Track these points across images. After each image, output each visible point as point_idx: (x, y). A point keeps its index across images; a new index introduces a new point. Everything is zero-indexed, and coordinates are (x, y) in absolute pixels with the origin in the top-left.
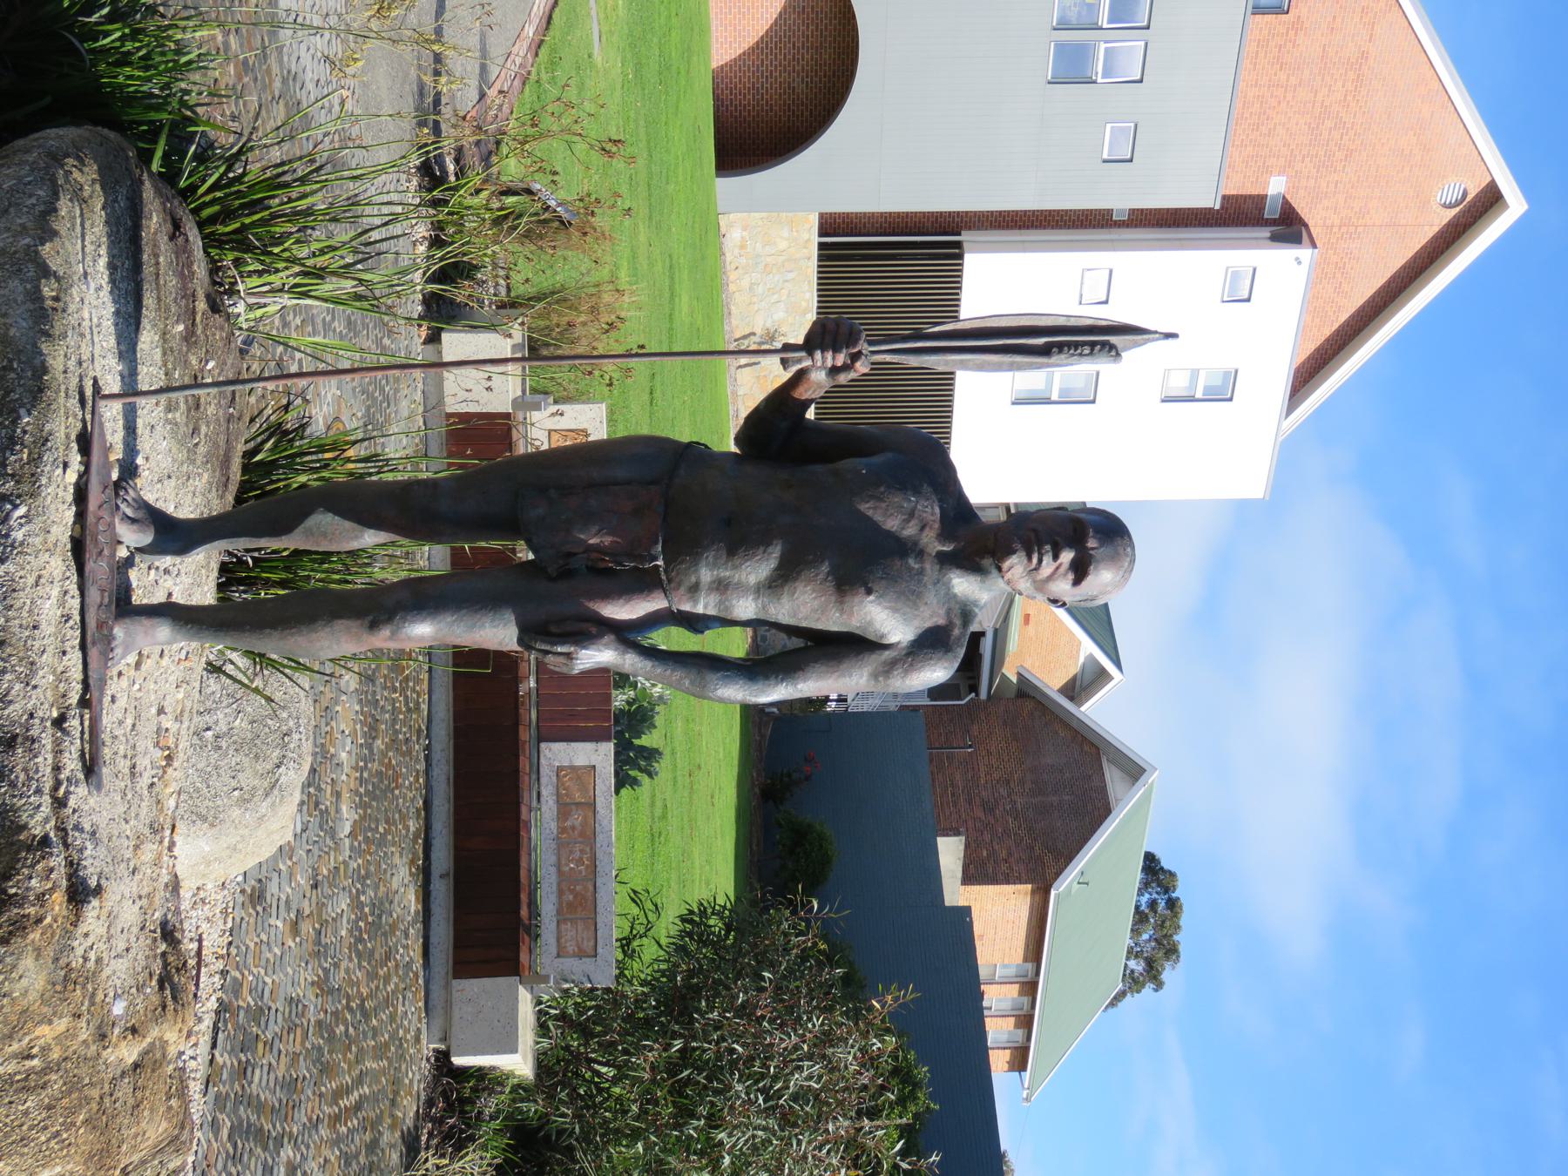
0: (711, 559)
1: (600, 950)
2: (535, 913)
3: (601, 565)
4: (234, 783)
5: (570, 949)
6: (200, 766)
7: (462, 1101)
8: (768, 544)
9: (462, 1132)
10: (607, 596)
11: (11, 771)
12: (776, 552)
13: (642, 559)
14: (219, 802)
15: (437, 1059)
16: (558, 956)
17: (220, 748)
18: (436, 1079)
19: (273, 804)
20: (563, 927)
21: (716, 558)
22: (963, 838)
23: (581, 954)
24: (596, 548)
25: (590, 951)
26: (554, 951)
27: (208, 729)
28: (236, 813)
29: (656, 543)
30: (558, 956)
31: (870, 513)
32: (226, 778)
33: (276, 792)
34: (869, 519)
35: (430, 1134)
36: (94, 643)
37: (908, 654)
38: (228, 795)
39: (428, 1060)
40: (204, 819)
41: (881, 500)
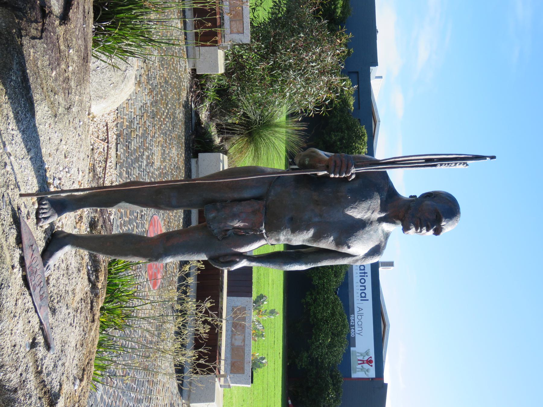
0: (284, 233)
1: (245, 31)
2: (221, 345)
3: (240, 234)
4: (110, 82)
5: (235, 31)
6: (97, 81)
7: (202, 85)
8: (308, 230)
9: (202, 94)
10: (242, 246)
11: (18, 399)
12: (311, 233)
13: (256, 231)
14: (106, 90)
15: (192, 72)
16: (231, 33)
17: (103, 72)
18: (193, 78)
19: (126, 84)
20: (232, 23)
21: (286, 233)
22: (371, 68)
23: (238, 33)
24: (238, 228)
25: (241, 31)
26: (229, 32)
27: (98, 67)
28: (113, 92)
29: (262, 226)
30: (231, 33)
31: (351, 214)
32: (107, 82)
33: (126, 80)
34: (350, 216)
35: (192, 97)
36: (40, 307)
37: (363, 258)
38: (109, 87)
39: (189, 73)
40: (101, 97)
41: (356, 208)
